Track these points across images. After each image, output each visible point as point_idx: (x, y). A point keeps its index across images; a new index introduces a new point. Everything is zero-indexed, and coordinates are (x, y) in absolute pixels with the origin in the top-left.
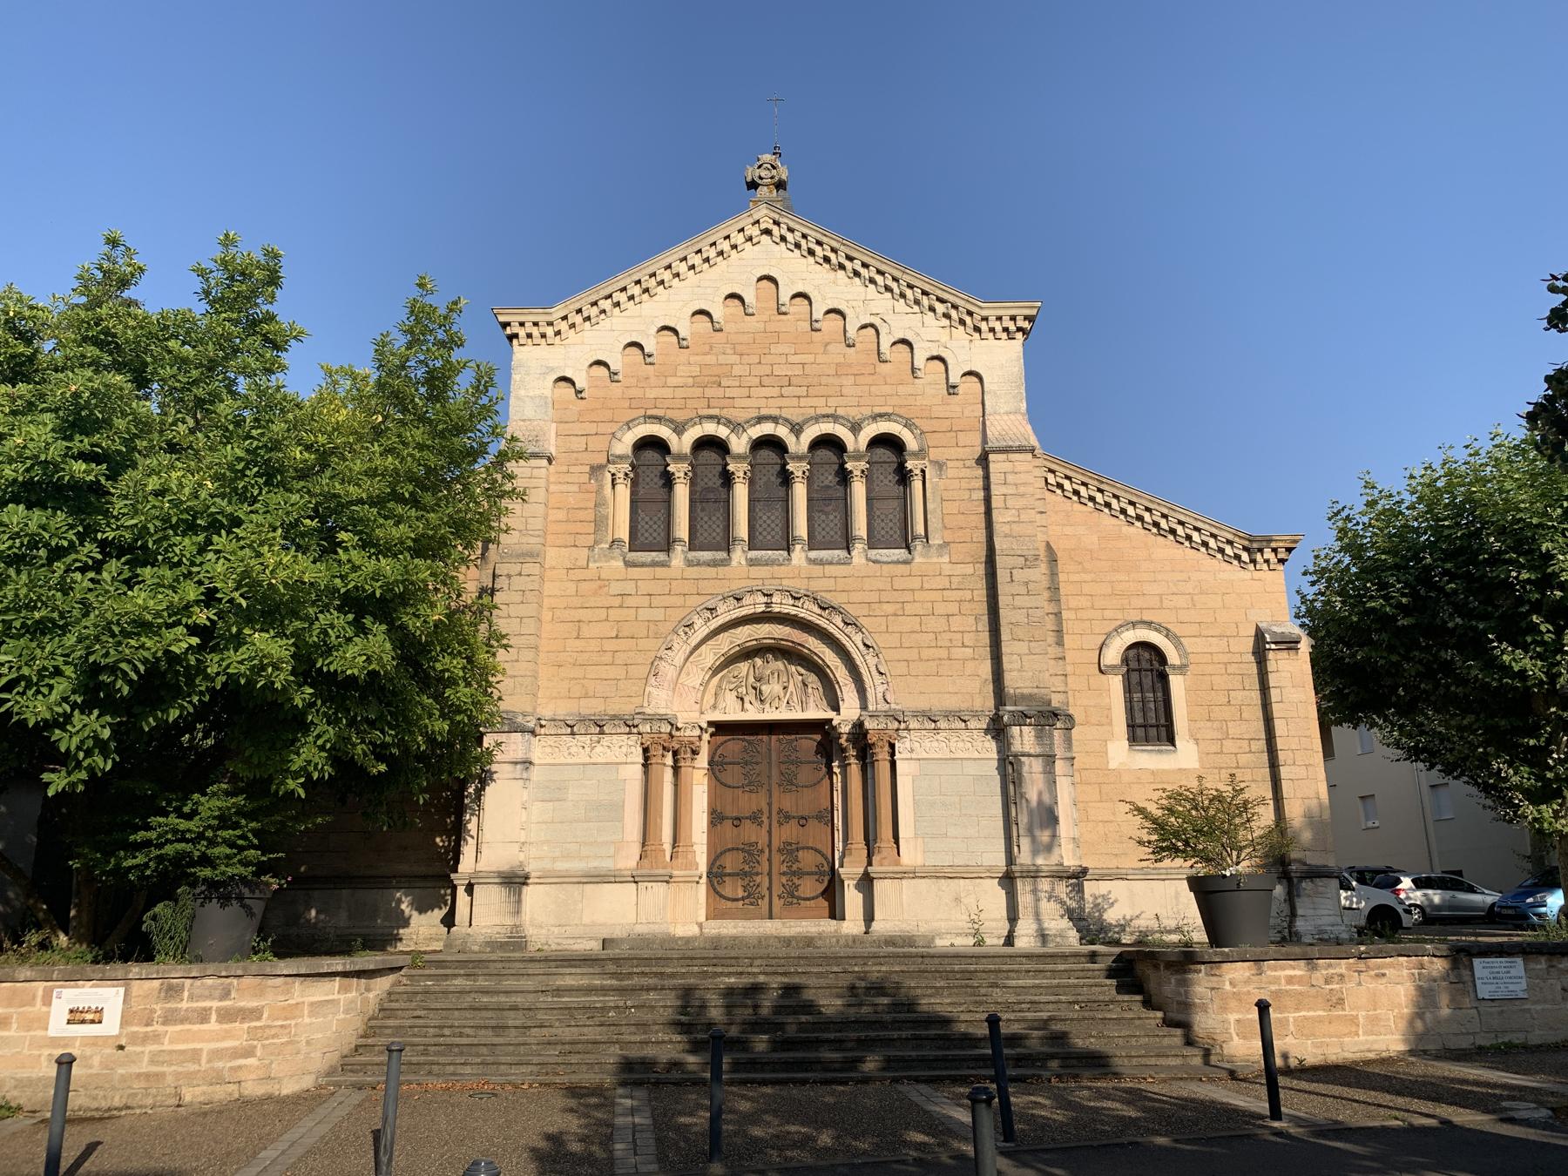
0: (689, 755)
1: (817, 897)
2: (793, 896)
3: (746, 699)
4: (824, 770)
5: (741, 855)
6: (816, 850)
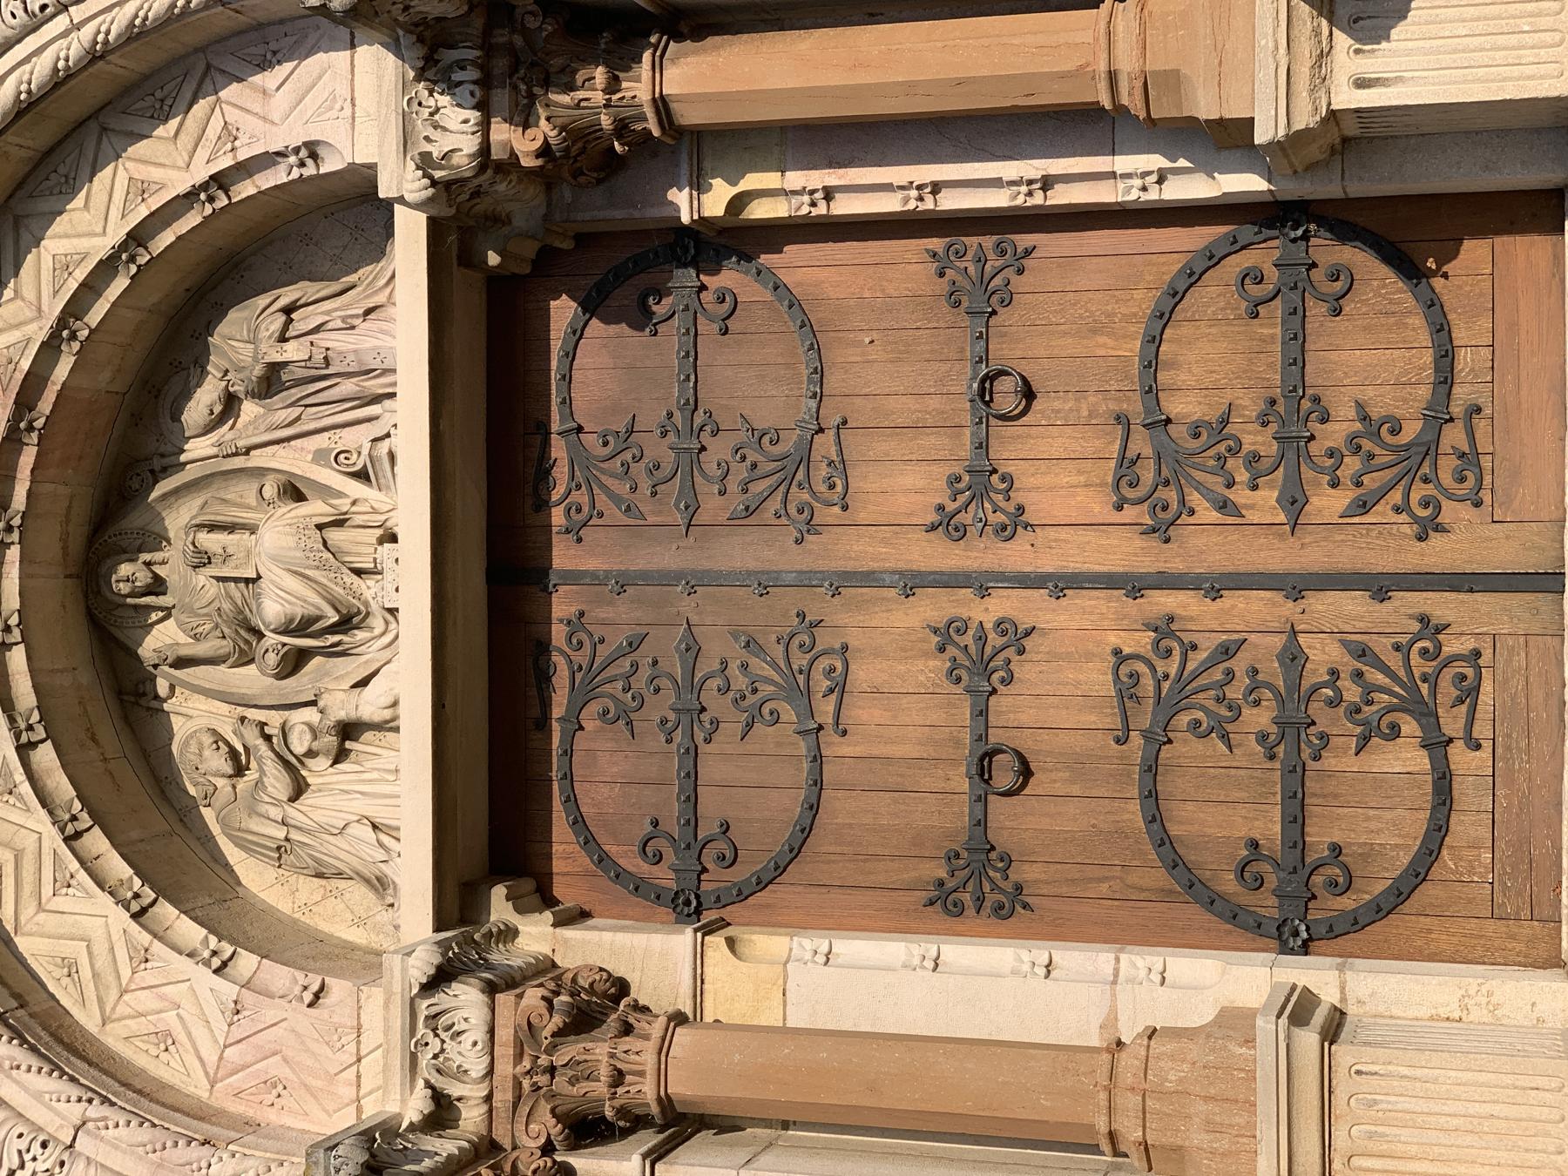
0: (598, 1050)
1: (1433, 307)
2: (1428, 448)
3: (342, 706)
4: (729, 278)
5: (1185, 749)
6: (1164, 317)
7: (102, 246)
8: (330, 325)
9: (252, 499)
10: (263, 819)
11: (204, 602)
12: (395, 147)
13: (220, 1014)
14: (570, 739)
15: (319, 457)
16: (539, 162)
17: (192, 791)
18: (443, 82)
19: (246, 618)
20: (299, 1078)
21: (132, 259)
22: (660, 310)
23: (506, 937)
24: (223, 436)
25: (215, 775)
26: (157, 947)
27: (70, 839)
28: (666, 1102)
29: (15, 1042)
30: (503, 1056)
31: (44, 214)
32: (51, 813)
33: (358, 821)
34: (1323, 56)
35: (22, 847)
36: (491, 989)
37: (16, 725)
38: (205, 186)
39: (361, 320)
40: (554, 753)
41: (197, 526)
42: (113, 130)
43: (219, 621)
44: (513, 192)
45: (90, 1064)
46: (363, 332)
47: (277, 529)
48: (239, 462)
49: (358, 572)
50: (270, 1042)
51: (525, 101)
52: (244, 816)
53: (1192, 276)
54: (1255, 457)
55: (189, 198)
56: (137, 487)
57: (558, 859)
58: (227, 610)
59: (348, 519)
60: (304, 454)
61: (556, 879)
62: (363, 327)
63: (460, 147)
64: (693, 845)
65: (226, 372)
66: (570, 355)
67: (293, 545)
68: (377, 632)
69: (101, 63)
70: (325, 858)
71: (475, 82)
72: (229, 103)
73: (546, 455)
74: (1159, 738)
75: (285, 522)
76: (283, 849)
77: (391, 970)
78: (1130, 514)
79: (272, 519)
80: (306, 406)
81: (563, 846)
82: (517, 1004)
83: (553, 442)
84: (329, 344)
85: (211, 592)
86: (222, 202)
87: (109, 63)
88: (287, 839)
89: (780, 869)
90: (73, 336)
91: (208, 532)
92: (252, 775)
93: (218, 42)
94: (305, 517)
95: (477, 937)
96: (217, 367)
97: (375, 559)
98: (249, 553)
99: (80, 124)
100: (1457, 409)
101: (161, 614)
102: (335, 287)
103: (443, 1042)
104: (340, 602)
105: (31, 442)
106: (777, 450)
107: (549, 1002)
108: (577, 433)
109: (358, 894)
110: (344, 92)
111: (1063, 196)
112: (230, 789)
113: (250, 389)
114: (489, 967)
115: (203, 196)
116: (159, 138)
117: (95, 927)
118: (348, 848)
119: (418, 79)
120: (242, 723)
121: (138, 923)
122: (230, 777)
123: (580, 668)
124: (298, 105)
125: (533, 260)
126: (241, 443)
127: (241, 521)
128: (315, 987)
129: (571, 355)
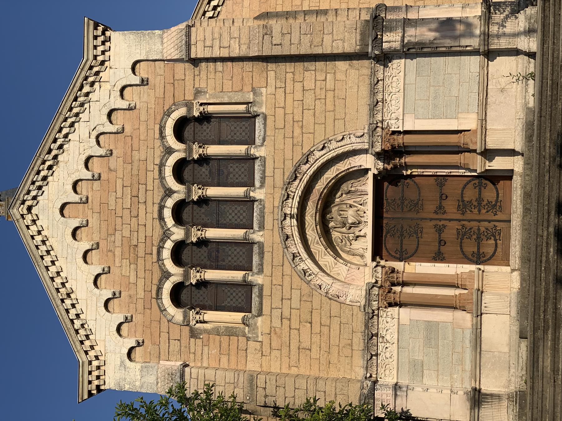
1: (496, 189)
2: (495, 205)
3: (357, 234)
4: (408, 181)
5: (465, 240)
6: (464, 188)
7: (333, 176)
9: (345, 207)
15: (354, 202)
22: (399, 184)
27: (326, 249)
28: (403, 281)
34: (485, 163)
53: (468, 183)
54: (475, 206)
62: (362, 186)
64: (402, 252)
66: (387, 190)
74: (462, 239)
78: (459, 212)
89: (413, 255)
100: (499, 201)
106: (414, 203)
111: (452, 174)
117: (329, 261)
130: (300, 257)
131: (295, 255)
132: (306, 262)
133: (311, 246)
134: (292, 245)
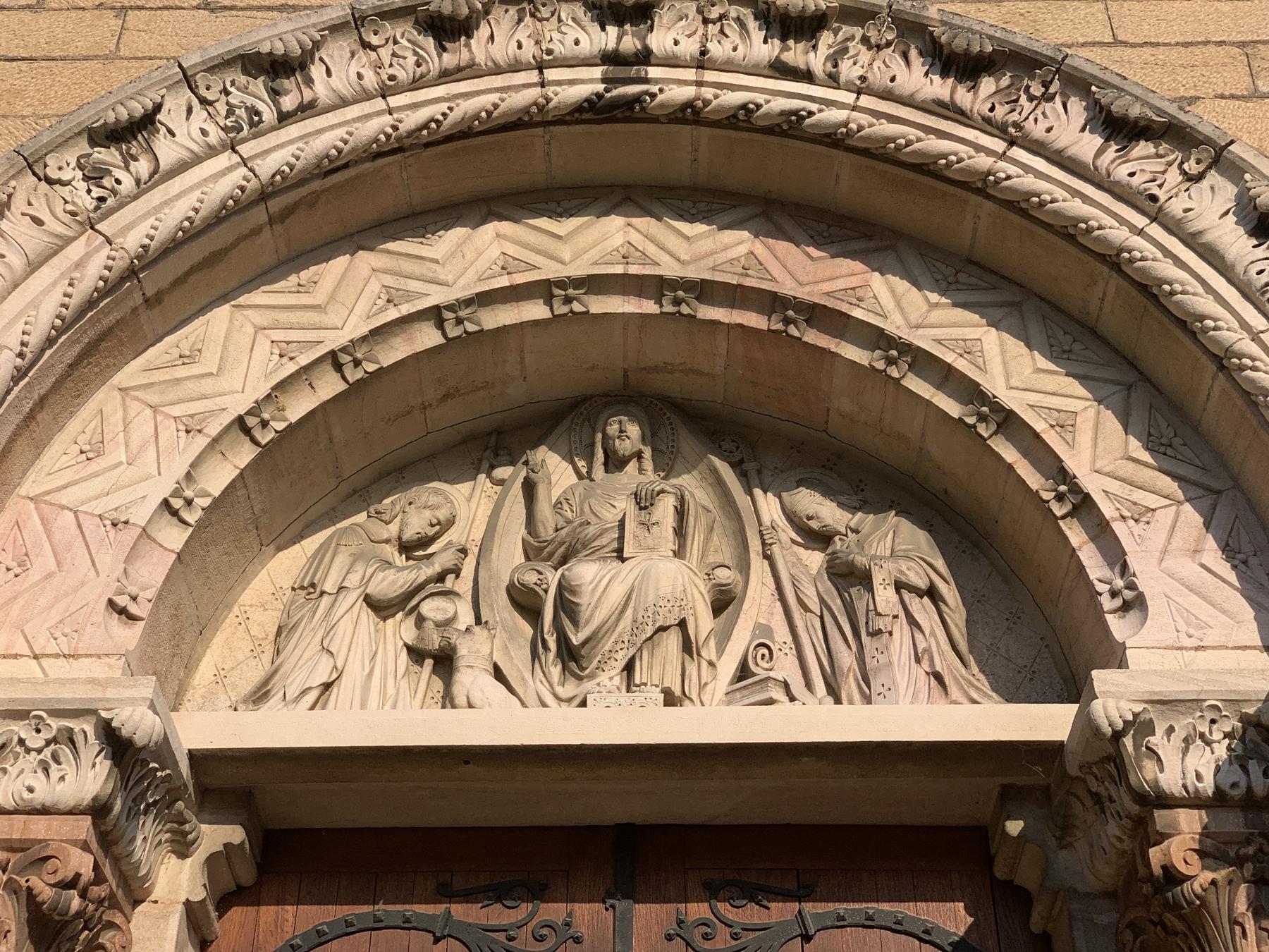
7: (995, 385)
8: (918, 636)
9: (713, 559)
10: (347, 568)
11: (597, 508)
12: (1157, 689)
13: (114, 506)
14: (424, 926)
16: (1157, 870)
17: (387, 501)
18: (1245, 750)
19: (578, 552)
20: (26, 590)
21: (982, 418)
23: (178, 842)
24: (783, 530)
25: (402, 521)
26: (202, 442)
27: (333, 359)
29: (101, 283)
30: (11, 826)
31: (1025, 329)
32: (364, 339)
33: (335, 667)
35: (329, 312)
36: (98, 810)
37: (463, 307)
38: (1075, 489)
39: (928, 670)
40: (408, 907)
41: (682, 497)
42: (1129, 396)
43: (575, 524)
44: (1105, 844)
45: (72, 366)
46: (914, 671)
47: (680, 576)
48: (755, 545)
49: (629, 668)
50: (73, 559)
51: (1232, 854)
52: (353, 549)
55: (1060, 473)
56: (724, 447)
57: (277, 913)
58: (586, 532)
59: (692, 657)
60: (766, 615)
61: (251, 910)
62: (920, 672)
63: (1166, 770)
65: (856, 531)
66: (898, 927)
67: (661, 593)
68: (559, 690)
69: (1213, 368)
70: (297, 635)
71: (1249, 788)
72: (1178, 514)
73: (773, 896)
75: (687, 586)
76: (312, 590)
77: (134, 686)
79: (691, 574)
80: (822, 618)
81: (291, 919)
82: (74, 843)
83: (789, 904)
84: (896, 635)
85: (608, 514)
86: (1058, 510)
87: (1214, 379)
88: (323, 593)
90: (891, 361)
91: (676, 507)
92: (400, 560)
93: (1248, 501)
94: (694, 608)
95: (180, 805)
96: (861, 521)
97: (645, 684)
98: (651, 549)
99: (1132, 364)
101: (584, 471)
102: (963, 646)
103: (39, 751)
104: (594, 647)
105: (772, 323)
107: (71, 884)
108: (801, 935)
109: (253, 674)
110: (1210, 638)
112: (385, 536)
113: (839, 555)
114: (132, 813)
115: (1063, 488)
116: (1126, 443)
117: (233, 380)
118: (306, 656)
119: (1244, 719)
120: (460, 551)
121: (232, 423)
122: (400, 538)
123: (511, 939)
124: (1187, 587)
125: (1012, 881)
126: (776, 549)
127: (689, 542)
128: (133, 609)
129: (898, 927)
130: (269, 115)
131: (288, 83)
132: (225, 159)
133: (366, 260)
134: (378, 66)
